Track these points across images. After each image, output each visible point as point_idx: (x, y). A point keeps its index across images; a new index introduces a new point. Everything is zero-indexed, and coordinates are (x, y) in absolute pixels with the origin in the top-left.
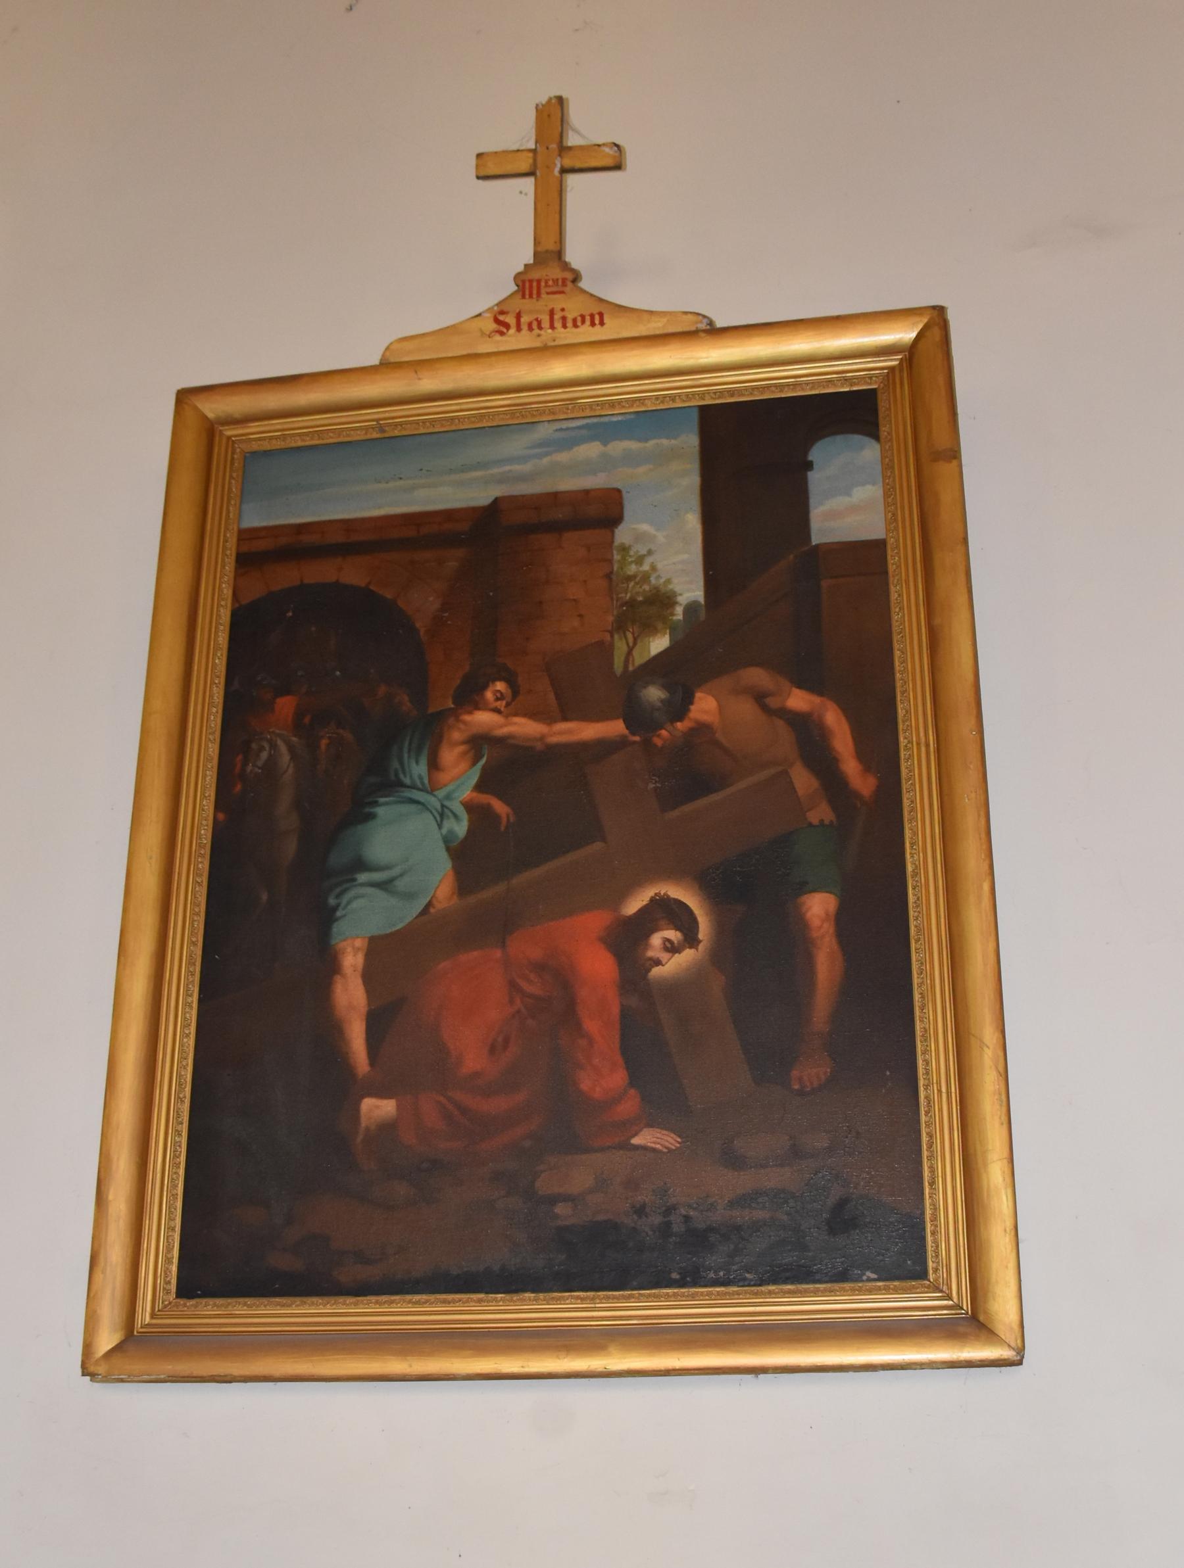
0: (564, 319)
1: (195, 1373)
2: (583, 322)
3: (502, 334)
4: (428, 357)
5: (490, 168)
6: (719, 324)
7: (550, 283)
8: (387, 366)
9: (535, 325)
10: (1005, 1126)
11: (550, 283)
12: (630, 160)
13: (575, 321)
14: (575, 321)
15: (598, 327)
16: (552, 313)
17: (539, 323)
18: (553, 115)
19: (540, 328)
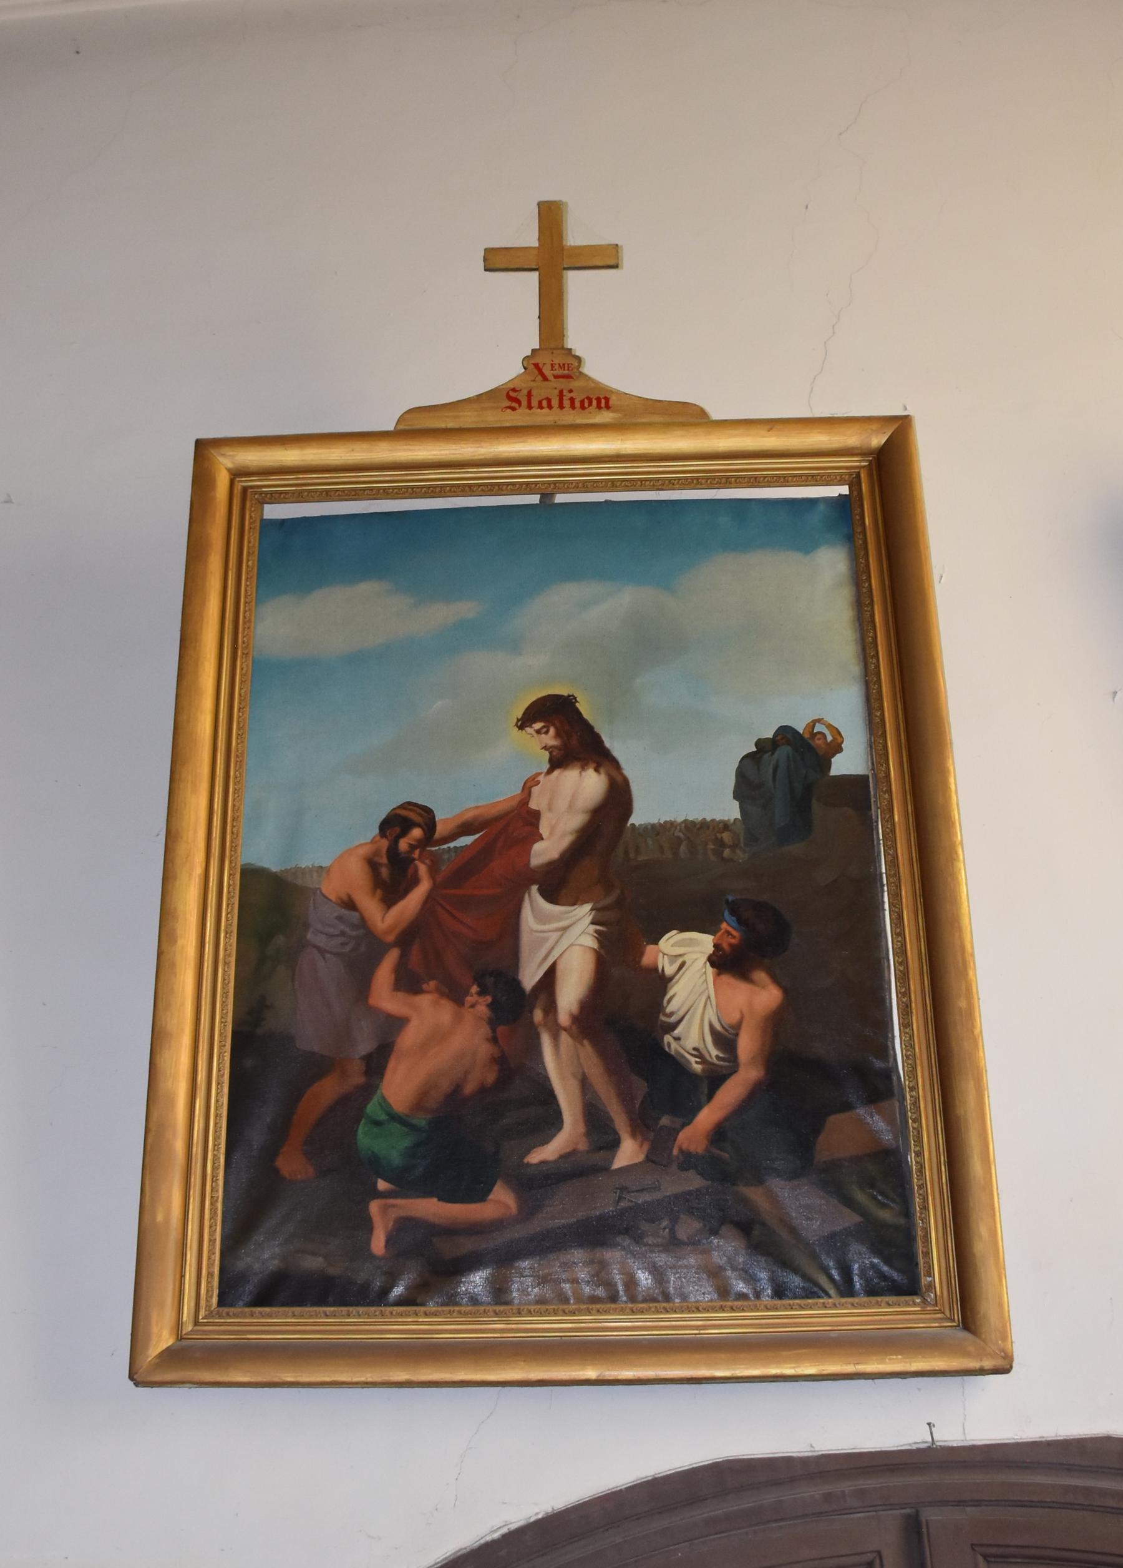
0: (572, 400)
1: (276, 1380)
2: (590, 404)
3: (514, 409)
4: (443, 426)
5: (497, 260)
6: (715, 416)
7: (557, 367)
8: (411, 428)
9: (545, 403)
10: (156, 1028)
11: (557, 367)
12: (627, 259)
13: (582, 402)
14: (540, 402)
15: (546, 411)
16: (561, 395)
17: (549, 401)
18: (550, 216)
19: (550, 407)
